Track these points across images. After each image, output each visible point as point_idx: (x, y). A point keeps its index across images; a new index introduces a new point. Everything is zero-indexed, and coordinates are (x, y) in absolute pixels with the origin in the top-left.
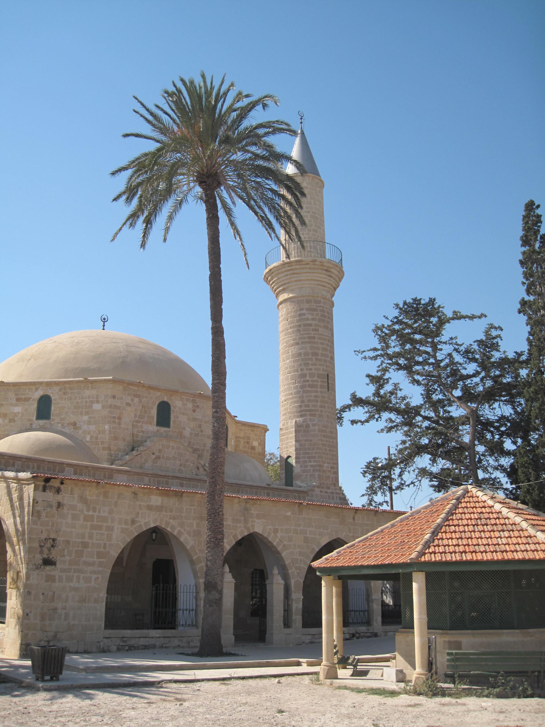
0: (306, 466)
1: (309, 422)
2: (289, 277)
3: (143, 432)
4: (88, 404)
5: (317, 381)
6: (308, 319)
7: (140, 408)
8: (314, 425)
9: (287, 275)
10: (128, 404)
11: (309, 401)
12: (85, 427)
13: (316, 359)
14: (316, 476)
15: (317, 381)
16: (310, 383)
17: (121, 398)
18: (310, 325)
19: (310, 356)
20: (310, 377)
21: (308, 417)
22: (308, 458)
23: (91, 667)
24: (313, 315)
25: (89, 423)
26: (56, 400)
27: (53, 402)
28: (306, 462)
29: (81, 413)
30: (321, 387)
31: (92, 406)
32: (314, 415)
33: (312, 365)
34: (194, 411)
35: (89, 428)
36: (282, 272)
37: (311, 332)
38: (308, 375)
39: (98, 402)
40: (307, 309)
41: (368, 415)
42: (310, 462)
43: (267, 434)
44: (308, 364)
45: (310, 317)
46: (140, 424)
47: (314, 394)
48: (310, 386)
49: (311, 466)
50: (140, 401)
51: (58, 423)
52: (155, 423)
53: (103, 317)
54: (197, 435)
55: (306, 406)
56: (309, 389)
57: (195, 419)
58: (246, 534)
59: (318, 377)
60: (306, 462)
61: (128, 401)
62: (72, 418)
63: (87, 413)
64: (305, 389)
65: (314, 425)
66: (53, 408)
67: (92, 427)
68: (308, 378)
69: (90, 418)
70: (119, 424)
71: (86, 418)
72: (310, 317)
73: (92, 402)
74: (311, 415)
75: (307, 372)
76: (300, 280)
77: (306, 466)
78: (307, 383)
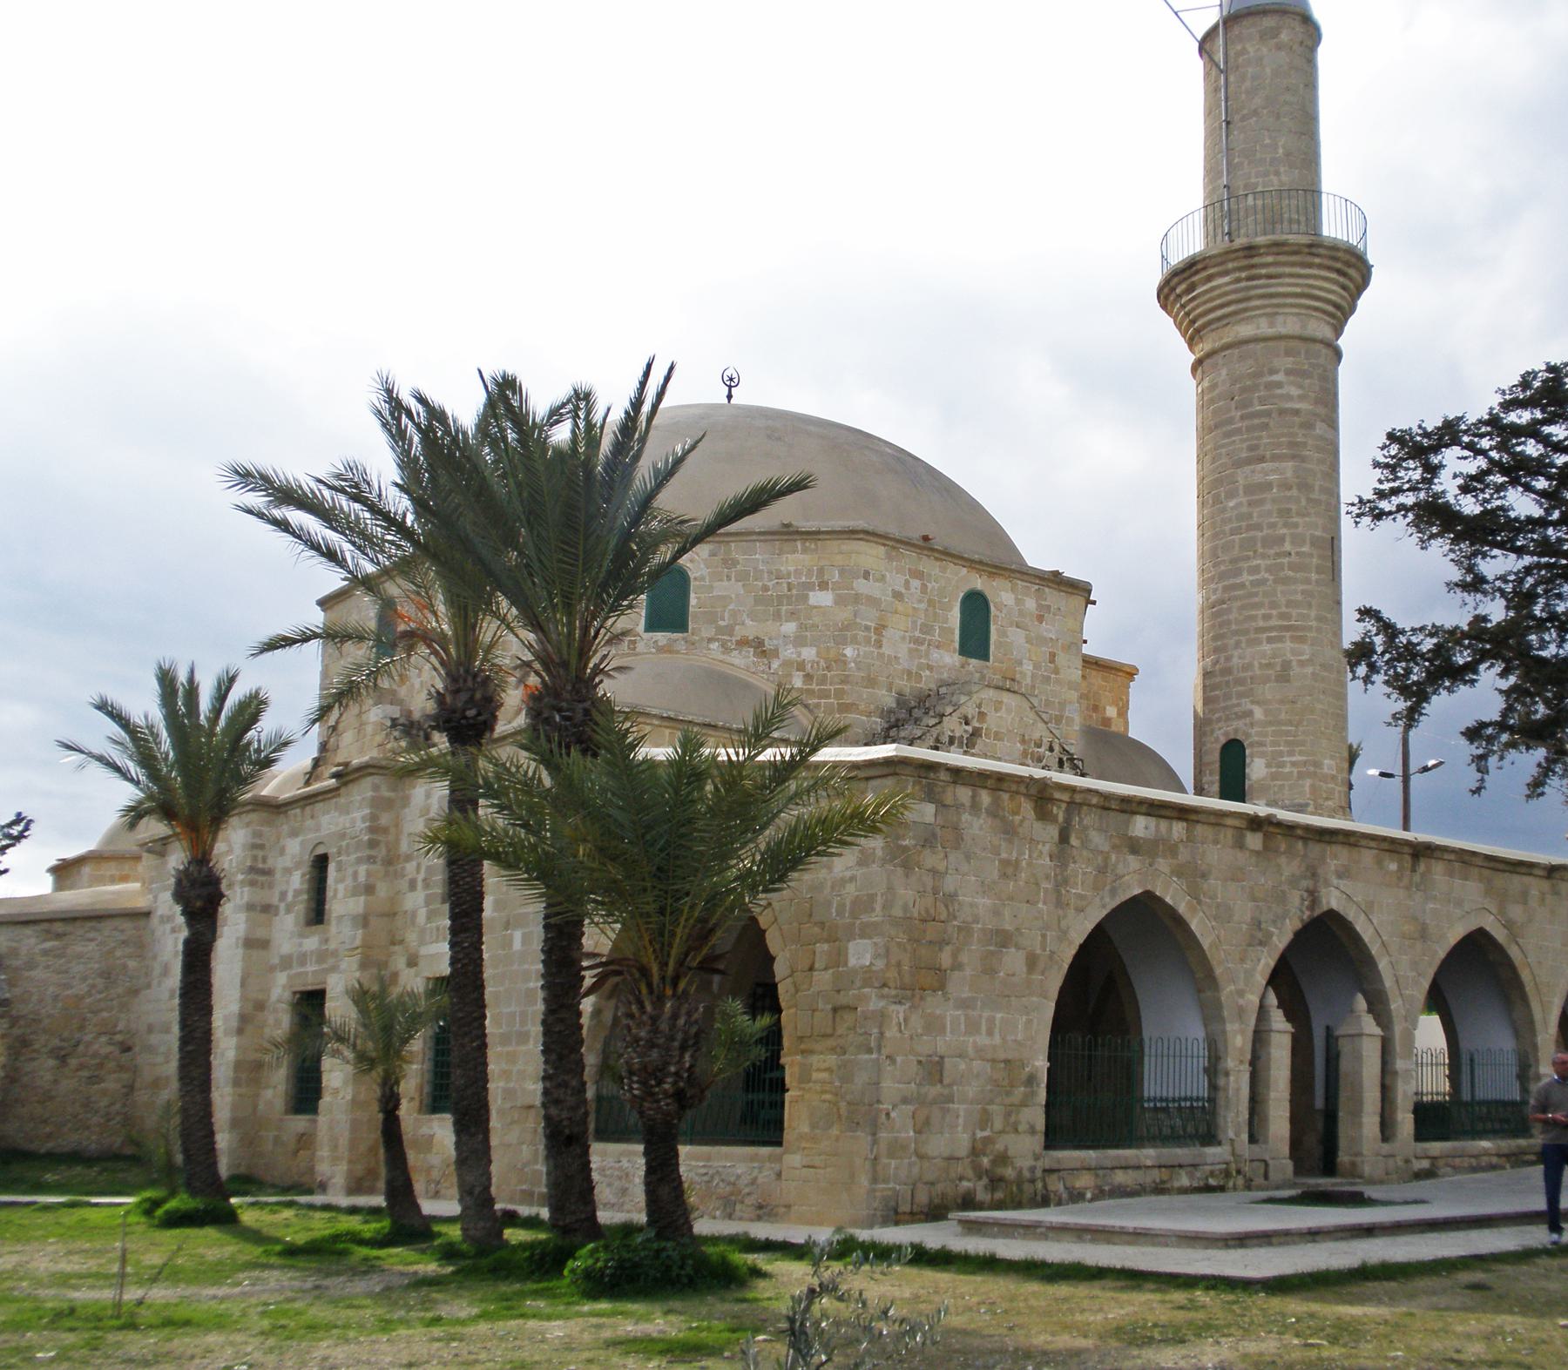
0: (1282, 765)
1: (1289, 656)
2: (1243, 284)
3: (930, 668)
4: (794, 592)
5: (1311, 555)
6: (1289, 398)
7: (923, 606)
8: (1302, 664)
9: (1238, 280)
10: (898, 595)
11: (1289, 604)
12: (788, 653)
13: (1309, 500)
14: (1307, 789)
15: (1311, 555)
16: (1294, 558)
17: (882, 579)
18: (1297, 412)
19: (1295, 492)
20: (1293, 543)
21: (1289, 644)
22: (1288, 743)
23: (1380, 1302)
24: (1300, 387)
25: (799, 641)
26: (702, 578)
27: (693, 584)
28: (1281, 754)
29: (777, 616)
30: (1319, 570)
31: (806, 597)
32: (1301, 640)
33: (1299, 514)
34: (1040, 619)
35: (799, 655)
36: (1226, 273)
37: (1296, 429)
38: (1288, 539)
39: (823, 586)
40: (1288, 372)
41: (142, 722)
42: (1291, 753)
43: (1134, 687)
44: (1289, 510)
45: (1294, 391)
46: (923, 648)
47: (1301, 587)
48: (1292, 567)
49: (1294, 764)
50: (924, 588)
51: (710, 640)
52: (957, 645)
53: (728, 373)
54: (1047, 680)
55: (1282, 616)
56: (1291, 573)
57: (1043, 641)
58: (448, 923)
59: (1312, 544)
60: (1281, 754)
61: (897, 588)
62: (750, 629)
63: (792, 615)
64: (1281, 574)
65: (1302, 664)
66: (693, 601)
67: (809, 653)
68: (1287, 547)
69: (801, 627)
70: (879, 644)
71: (790, 628)
72: (1294, 391)
73: (809, 587)
74: (1294, 639)
75: (1284, 531)
76: (1272, 296)
77: (1282, 765)
78: (1286, 560)
